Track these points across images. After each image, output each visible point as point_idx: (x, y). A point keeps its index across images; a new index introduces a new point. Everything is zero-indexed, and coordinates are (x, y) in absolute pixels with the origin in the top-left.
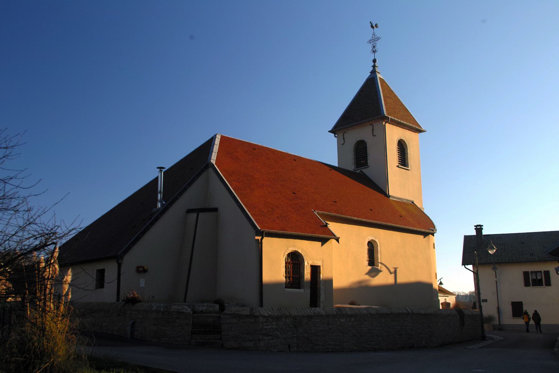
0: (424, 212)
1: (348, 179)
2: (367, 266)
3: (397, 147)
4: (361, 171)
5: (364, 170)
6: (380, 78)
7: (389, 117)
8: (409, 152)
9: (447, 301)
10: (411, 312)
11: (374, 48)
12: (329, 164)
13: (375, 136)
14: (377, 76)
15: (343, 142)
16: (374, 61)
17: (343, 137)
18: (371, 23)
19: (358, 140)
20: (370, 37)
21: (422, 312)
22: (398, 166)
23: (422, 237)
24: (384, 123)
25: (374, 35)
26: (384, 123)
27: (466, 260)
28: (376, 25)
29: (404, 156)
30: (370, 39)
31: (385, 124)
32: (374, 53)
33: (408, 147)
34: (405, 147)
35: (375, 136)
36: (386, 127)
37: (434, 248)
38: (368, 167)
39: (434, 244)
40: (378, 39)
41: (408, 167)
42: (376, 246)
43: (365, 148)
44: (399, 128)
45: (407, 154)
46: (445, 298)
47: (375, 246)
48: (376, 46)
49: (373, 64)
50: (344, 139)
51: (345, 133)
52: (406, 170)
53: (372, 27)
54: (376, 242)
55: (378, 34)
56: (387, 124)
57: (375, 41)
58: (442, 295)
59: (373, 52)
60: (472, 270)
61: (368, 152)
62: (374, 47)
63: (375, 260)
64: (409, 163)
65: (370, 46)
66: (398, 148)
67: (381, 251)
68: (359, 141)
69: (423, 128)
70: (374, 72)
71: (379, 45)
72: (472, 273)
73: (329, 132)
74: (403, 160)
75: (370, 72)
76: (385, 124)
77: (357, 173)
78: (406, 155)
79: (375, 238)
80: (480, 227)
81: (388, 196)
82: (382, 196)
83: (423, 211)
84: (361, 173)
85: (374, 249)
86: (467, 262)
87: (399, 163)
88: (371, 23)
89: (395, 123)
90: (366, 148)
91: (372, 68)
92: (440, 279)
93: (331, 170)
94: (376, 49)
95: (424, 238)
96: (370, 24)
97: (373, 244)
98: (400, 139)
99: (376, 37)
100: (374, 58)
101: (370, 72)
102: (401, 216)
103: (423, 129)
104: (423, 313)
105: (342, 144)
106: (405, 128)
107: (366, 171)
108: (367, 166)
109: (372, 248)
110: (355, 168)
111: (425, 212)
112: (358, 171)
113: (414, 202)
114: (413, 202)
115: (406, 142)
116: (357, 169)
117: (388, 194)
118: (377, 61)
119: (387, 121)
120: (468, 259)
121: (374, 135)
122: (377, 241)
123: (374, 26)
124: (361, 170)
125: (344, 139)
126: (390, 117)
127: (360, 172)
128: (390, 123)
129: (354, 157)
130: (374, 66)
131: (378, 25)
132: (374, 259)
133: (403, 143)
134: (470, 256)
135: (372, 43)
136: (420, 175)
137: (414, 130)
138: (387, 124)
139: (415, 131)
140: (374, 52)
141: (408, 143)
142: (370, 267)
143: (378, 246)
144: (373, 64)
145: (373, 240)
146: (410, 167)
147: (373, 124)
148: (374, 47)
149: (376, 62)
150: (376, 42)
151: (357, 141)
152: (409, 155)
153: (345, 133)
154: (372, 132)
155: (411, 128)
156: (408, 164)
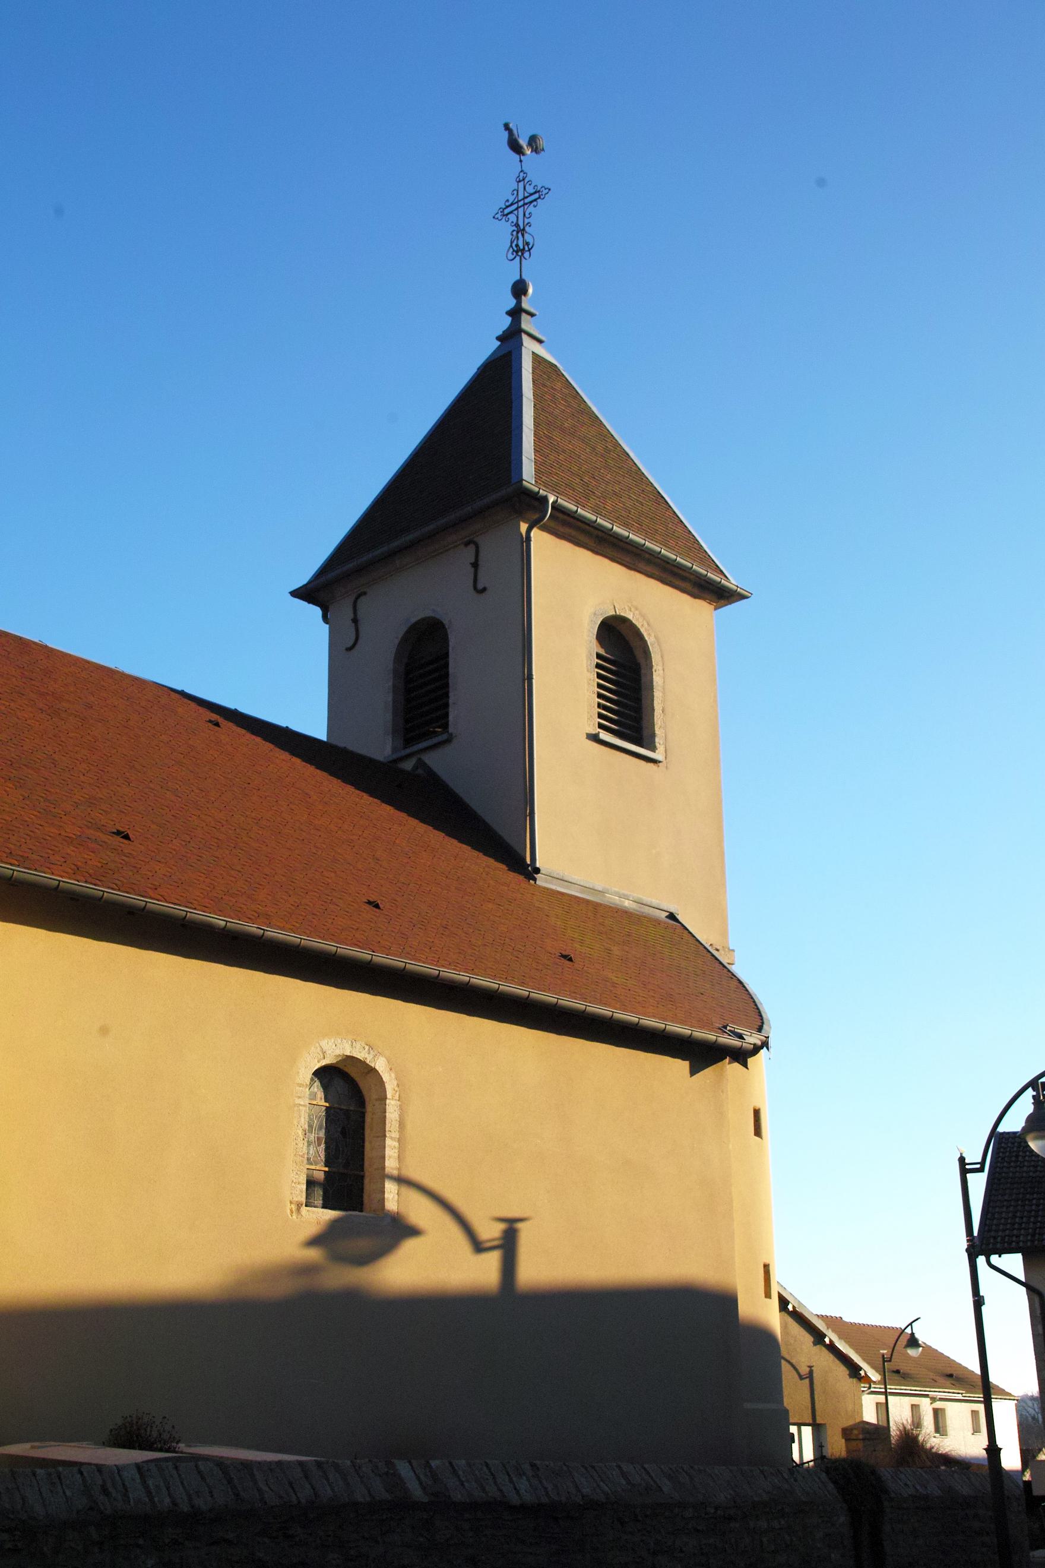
0: (734, 969)
2: (299, 1206)
4: (421, 764)
6: (537, 359)
7: (545, 499)
9: (865, 1419)
10: (417, 1492)
11: (520, 235)
12: (232, 706)
13: (484, 589)
15: (353, 638)
16: (519, 289)
17: (352, 616)
18: (507, 127)
19: (414, 620)
20: (504, 190)
21: (525, 1491)
22: (594, 738)
23: (683, 1066)
25: (521, 184)
26: (524, 527)
27: (997, 1231)
28: (533, 141)
29: (638, 700)
32: (518, 258)
33: (656, 658)
35: (484, 589)
37: (758, 1132)
38: (449, 741)
39: (757, 1113)
40: (539, 194)
41: (653, 748)
42: (374, 1096)
43: (442, 659)
44: (606, 561)
45: (651, 688)
46: (915, 1400)
47: (370, 1096)
48: (527, 228)
49: (512, 303)
50: (355, 621)
51: (363, 599)
52: (642, 763)
53: (515, 147)
54: (373, 1071)
55: (537, 178)
56: (535, 533)
58: (960, 1397)
59: (517, 252)
60: (1023, 1280)
61: (451, 670)
62: (520, 230)
63: (367, 1174)
65: (505, 229)
66: (599, 656)
67: (409, 1126)
68: (417, 623)
69: (733, 581)
70: (512, 337)
71: (540, 217)
72: (1024, 1289)
73: (295, 594)
74: (629, 727)
75: (498, 338)
77: (402, 771)
78: (644, 693)
79: (371, 1047)
80: (525, 544)
81: (530, 872)
82: (499, 870)
83: (725, 961)
84: (420, 771)
85: (363, 1115)
86: (999, 1239)
88: (507, 127)
89: (583, 538)
90: (447, 655)
91: (509, 319)
92: (911, 1324)
93: (217, 724)
94: (528, 238)
95: (692, 1072)
96: (506, 134)
97: (361, 1085)
98: (612, 613)
101: (498, 338)
102: (564, 957)
103: (733, 581)
104: (528, 1498)
107: (435, 760)
108: (444, 737)
109: (360, 1109)
110: (394, 750)
111: (736, 969)
112: (408, 765)
113: (679, 917)
114: (672, 916)
115: (642, 630)
116: (408, 751)
117: (528, 861)
118: (530, 291)
119: (536, 516)
120: (1004, 1231)
121: (480, 586)
122: (380, 1065)
123: (523, 142)
125: (355, 621)
126: (551, 499)
127: (416, 767)
128: (545, 529)
129: (394, 701)
130: (516, 313)
131: (542, 143)
132: (362, 1167)
134: (1015, 1217)
135: (513, 218)
137: (687, 586)
138: (535, 533)
139: (696, 590)
140: (520, 251)
141: (656, 637)
142: (323, 1216)
143: (389, 1095)
144: (512, 303)
145: (352, 1058)
146: (660, 748)
147: (475, 539)
148: (520, 230)
150: (511, 199)
152: (657, 694)
153: (365, 593)
154: (472, 576)
155: (675, 574)
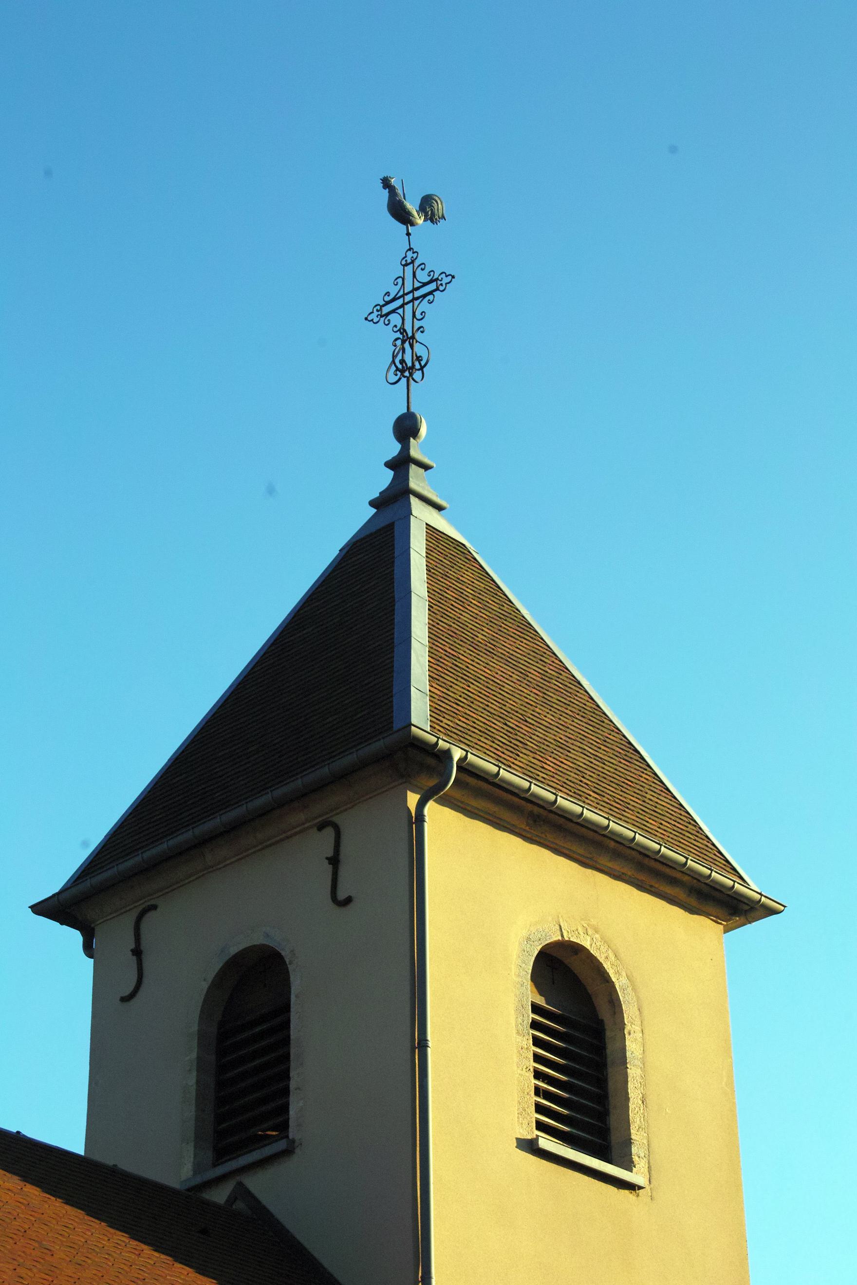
1: (55, 1206)
3: (532, 995)
4: (242, 1192)
5: (255, 1183)
6: (431, 531)
7: (448, 754)
8: (633, 1047)
13: (348, 901)
14: (410, 513)
18: (386, 183)
19: (234, 950)
22: (530, 1147)
24: (412, 799)
26: (412, 799)
28: (427, 204)
29: (601, 1082)
30: (388, 294)
31: (421, 805)
32: (404, 381)
33: (629, 1012)
34: (604, 1013)
35: (348, 901)
36: (427, 827)
38: (288, 1152)
48: (418, 336)
49: (394, 448)
56: (431, 809)
57: (414, 299)
59: (402, 371)
61: (294, 1032)
62: (407, 338)
64: (635, 1134)
66: (536, 1008)
73: (42, 909)
75: (372, 503)
76: (421, 805)
78: (611, 1071)
84: (239, 1205)
87: (540, 1126)
90: (286, 1008)
91: (390, 474)
94: (419, 350)
98: (557, 937)
99: (423, 277)
100: (405, 411)
101: (372, 503)
105: (125, 999)
106: (604, 861)
108: (282, 1145)
110: (198, 1168)
112: (220, 1196)
115: (607, 966)
119: (432, 782)
121: (341, 895)
123: (412, 206)
124: (240, 1184)
125: (137, 952)
126: (457, 754)
127: (232, 1199)
128: (447, 802)
133: (574, 963)
135: (395, 319)
136: (742, 1237)
138: (431, 809)
144: (394, 448)
146: (640, 1164)
147: (336, 819)
148: (407, 338)
149: (415, 433)
150: (424, 306)
151: (226, 958)
152: (633, 1072)
153: (154, 907)
156: (628, 1142)
